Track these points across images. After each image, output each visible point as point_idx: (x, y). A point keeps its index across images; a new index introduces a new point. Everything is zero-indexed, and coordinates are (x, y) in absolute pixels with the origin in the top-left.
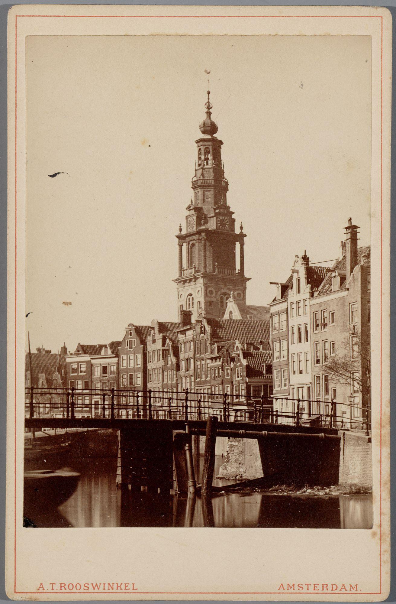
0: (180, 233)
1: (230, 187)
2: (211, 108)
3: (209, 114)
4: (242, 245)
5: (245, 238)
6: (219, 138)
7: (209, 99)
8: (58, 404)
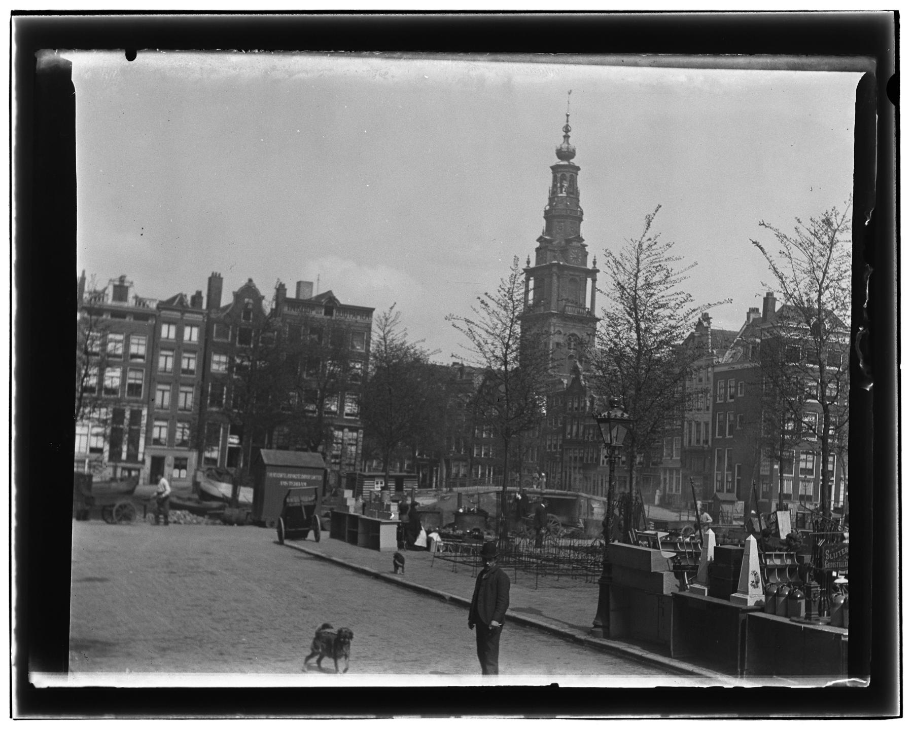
0: (528, 266)
1: (584, 218)
2: (570, 131)
3: (566, 137)
4: (594, 281)
5: (598, 274)
6: (577, 165)
7: (567, 121)
8: (459, 562)
